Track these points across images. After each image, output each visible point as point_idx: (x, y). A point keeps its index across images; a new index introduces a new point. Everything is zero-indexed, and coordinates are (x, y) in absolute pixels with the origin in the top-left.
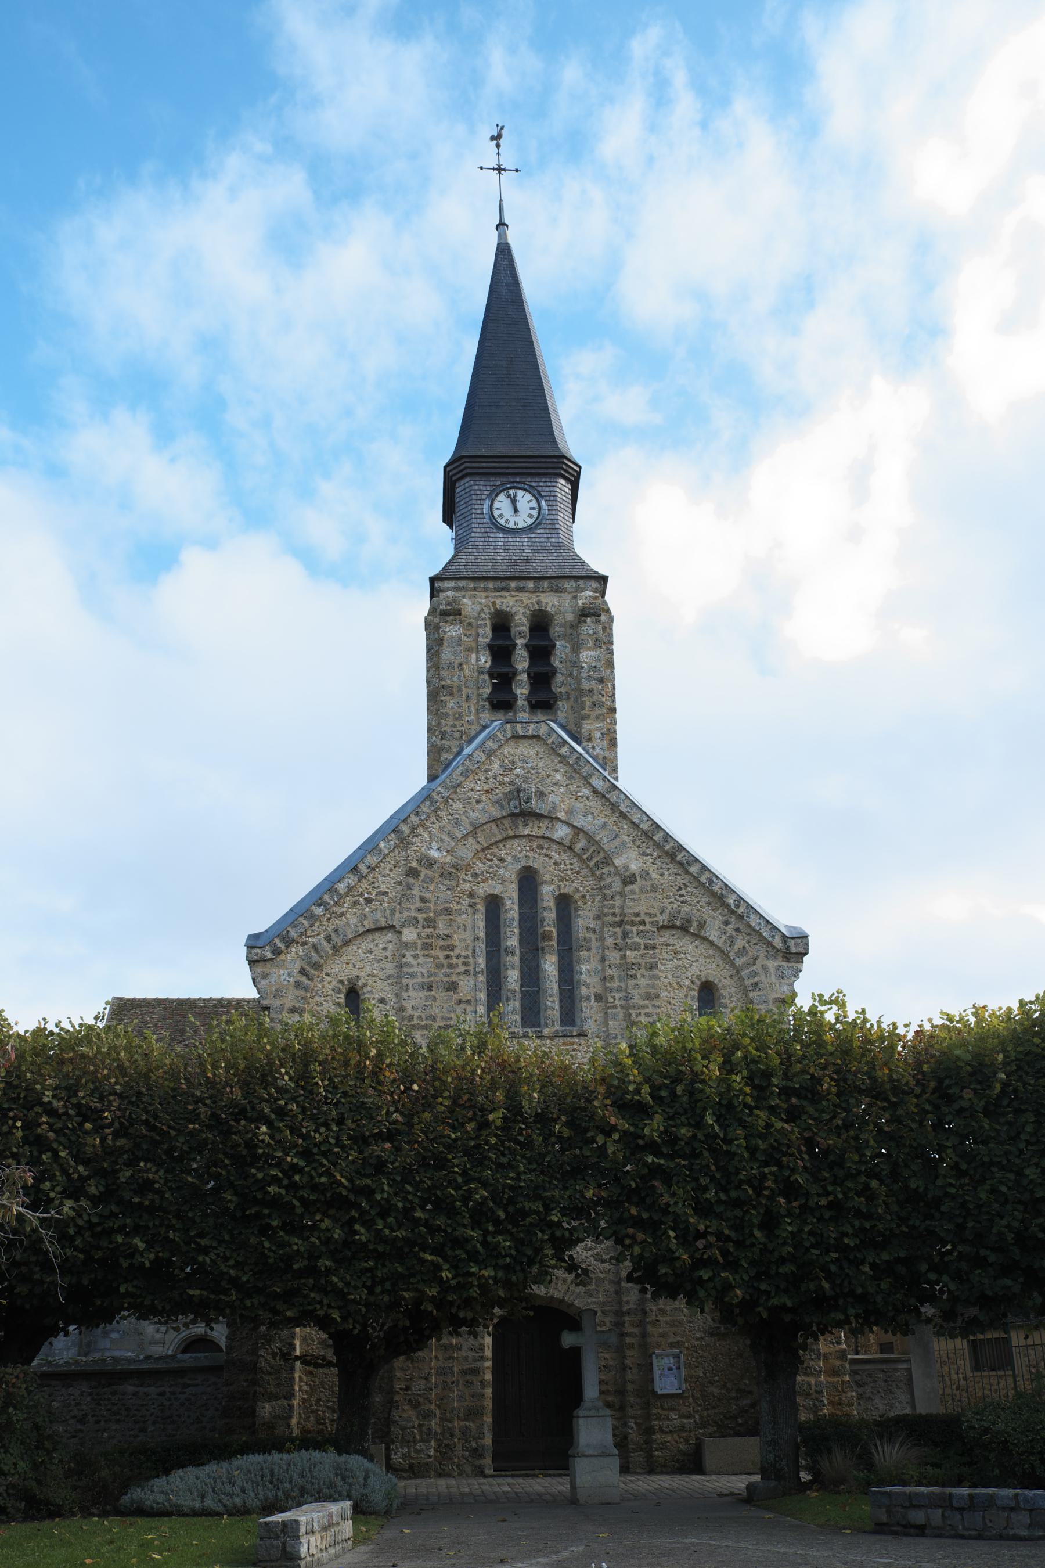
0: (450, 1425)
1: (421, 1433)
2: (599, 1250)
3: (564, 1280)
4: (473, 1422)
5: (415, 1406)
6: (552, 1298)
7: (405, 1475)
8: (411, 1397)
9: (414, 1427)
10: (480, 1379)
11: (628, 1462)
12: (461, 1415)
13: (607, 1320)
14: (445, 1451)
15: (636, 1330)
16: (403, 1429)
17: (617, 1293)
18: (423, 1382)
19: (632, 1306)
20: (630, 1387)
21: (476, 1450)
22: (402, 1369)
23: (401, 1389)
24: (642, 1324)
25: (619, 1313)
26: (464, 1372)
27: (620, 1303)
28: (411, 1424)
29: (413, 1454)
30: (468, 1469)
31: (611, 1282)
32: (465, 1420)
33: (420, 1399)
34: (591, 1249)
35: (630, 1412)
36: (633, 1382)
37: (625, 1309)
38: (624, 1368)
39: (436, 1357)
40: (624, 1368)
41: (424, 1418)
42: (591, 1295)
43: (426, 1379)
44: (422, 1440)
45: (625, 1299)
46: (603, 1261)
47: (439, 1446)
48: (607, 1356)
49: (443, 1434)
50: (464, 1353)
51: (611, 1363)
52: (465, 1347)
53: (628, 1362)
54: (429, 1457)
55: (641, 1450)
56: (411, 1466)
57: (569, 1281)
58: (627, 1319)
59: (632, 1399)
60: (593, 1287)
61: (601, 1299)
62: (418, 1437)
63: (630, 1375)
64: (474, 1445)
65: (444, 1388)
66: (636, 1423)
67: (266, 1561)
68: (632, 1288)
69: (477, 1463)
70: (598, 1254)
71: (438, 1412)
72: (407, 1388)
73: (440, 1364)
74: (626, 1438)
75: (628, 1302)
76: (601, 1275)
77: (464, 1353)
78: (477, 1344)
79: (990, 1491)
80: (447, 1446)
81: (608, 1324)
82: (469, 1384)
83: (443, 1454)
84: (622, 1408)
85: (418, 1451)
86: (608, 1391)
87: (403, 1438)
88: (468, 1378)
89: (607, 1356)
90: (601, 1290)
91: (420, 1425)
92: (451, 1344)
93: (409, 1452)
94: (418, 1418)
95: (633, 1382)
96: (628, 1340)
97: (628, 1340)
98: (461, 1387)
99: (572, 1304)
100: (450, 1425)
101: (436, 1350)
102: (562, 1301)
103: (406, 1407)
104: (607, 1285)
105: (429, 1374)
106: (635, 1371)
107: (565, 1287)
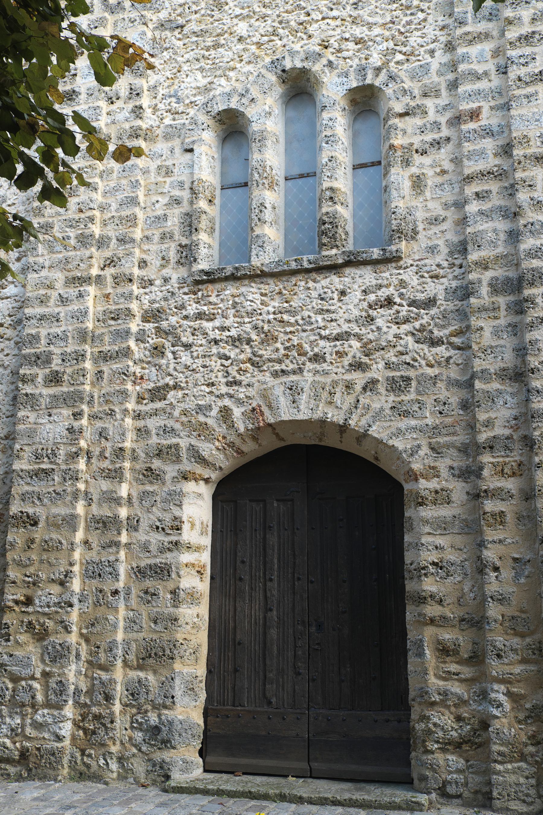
0: (104, 676)
1: (46, 688)
2: (425, 320)
3: (349, 386)
4: (155, 672)
5: (41, 635)
6: (323, 422)
7: (12, 770)
8: (32, 618)
9: (33, 678)
10: (171, 586)
11: (489, 783)
12: (132, 657)
13: (443, 465)
14: (93, 727)
15: (510, 484)
16: (15, 679)
17: (465, 405)
18: (56, 589)
19: (500, 431)
20: (494, 611)
21: (156, 730)
22: (19, 564)
23: (17, 602)
24: (523, 470)
25: (471, 449)
26: (140, 573)
27: (472, 427)
28: (28, 672)
29: (28, 730)
30: (139, 767)
31: (452, 383)
32: (140, 668)
33: (50, 624)
34: (407, 321)
35: (496, 667)
36: (501, 600)
37: (483, 437)
38: (481, 568)
39: (86, 542)
40: (481, 568)
41: (54, 660)
42: (406, 414)
43: (62, 584)
44: (48, 705)
45: (482, 416)
46: (434, 343)
47: (84, 717)
48: (440, 541)
49: (90, 692)
50: (141, 536)
51: (452, 556)
52: (144, 525)
53: (490, 554)
54: (59, 738)
55: (523, 757)
56: (24, 754)
57: (358, 388)
58: (486, 458)
59: (499, 640)
60: (412, 396)
61: (429, 421)
62: (40, 698)
63: (493, 584)
64: (153, 719)
65: (97, 604)
66: (508, 694)
67: (232, 795)
68: (500, 392)
69: (158, 756)
70: (422, 329)
71: (84, 649)
72: (29, 601)
73: (93, 555)
74: (485, 725)
75: (489, 424)
76: (430, 371)
77: (141, 536)
78: (167, 517)
79: (42, 165)
80: (98, 717)
81: (444, 473)
82: (149, 595)
83: (89, 733)
84: (476, 659)
85: (38, 726)
86: (444, 618)
87: (13, 696)
88: (149, 583)
89: (440, 541)
90: (429, 401)
91: (46, 675)
92: (116, 517)
93: (23, 726)
94: (43, 661)
95: (501, 600)
96: (489, 506)
97: (489, 506)
98: (134, 602)
99: (365, 435)
100: (104, 676)
101: (87, 529)
102: (343, 429)
103: (23, 638)
104: (442, 391)
105: (68, 574)
106: (507, 574)
107: (351, 399)
